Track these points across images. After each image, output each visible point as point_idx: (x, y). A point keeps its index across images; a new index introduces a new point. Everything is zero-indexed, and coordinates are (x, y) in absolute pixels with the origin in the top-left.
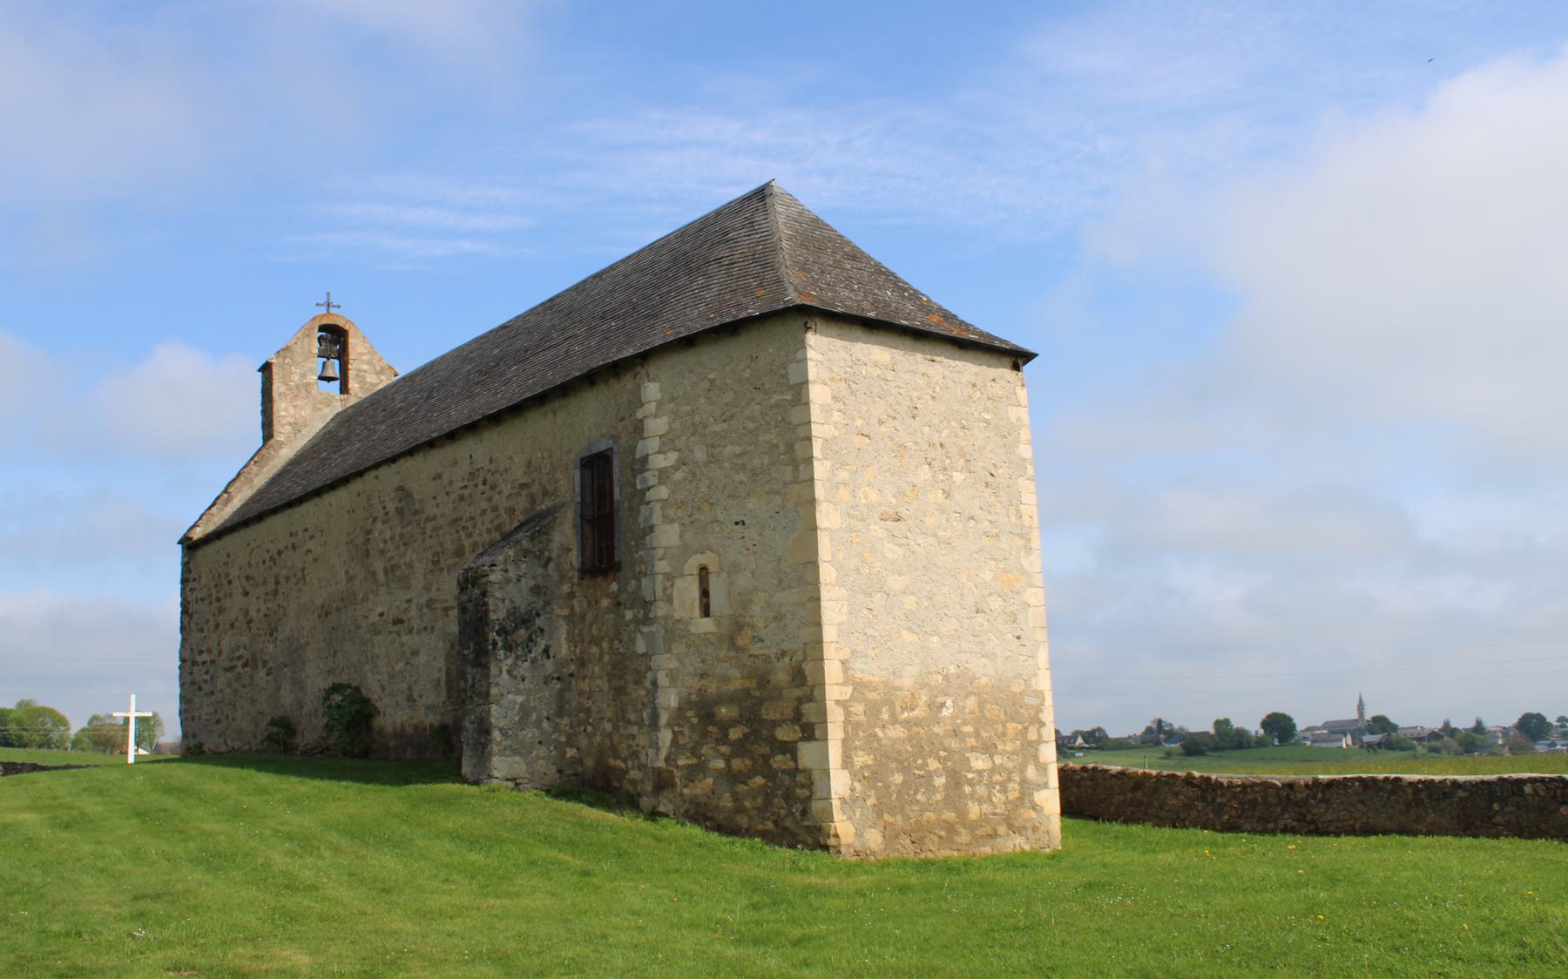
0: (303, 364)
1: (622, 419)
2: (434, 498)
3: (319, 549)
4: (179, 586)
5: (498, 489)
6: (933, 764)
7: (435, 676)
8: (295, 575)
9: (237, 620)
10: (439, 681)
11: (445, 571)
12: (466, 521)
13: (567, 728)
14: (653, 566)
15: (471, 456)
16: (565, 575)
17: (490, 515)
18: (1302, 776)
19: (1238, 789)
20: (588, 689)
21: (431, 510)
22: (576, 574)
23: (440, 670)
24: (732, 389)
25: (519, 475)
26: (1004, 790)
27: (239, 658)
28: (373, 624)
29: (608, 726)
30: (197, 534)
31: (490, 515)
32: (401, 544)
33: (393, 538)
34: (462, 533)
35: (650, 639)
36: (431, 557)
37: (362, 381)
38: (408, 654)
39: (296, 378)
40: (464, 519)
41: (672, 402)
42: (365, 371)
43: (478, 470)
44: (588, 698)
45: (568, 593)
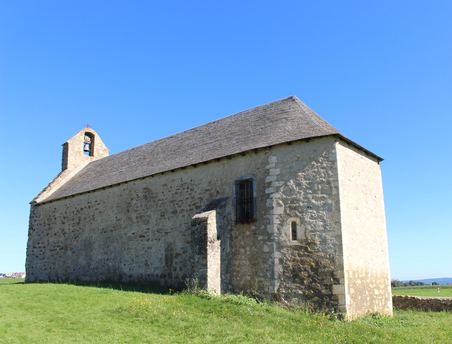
0: (79, 144)
1: (258, 169)
2: (163, 193)
3: (102, 208)
4: (28, 219)
5: (194, 191)
6: (367, 293)
7: (160, 256)
8: (89, 217)
9: (58, 232)
10: (161, 259)
11: (167, 219)
12: (178, 201)
13: (229, 278)
14: (273, 221)
15: (181, 178)
16: (229, 223)
17: (190, 200)
18: (433, 297)
19: (426, 301)
20: (238, 264)
21: (161, 196)
22: (233, 222)
23: (162, 255)
24: (306, 161)
25: (205, 185)
26: (381, 302)
27: (58, 246)
28: (129, 237)
29: (249, 278)
30: (38, 201)
31: (190, 200)
32: (145, 208)
33: (141, 206)
34: (176, 205)
35: (271, 247)
36: (160, 214)
37: (98, 153)
38: (146, 248)
39: (76, 149)
40: (177, 201)
41: (282, 164)
42: (99, 150)
43: (185, 184)
44: (238, 267)
45: (230, 229)
